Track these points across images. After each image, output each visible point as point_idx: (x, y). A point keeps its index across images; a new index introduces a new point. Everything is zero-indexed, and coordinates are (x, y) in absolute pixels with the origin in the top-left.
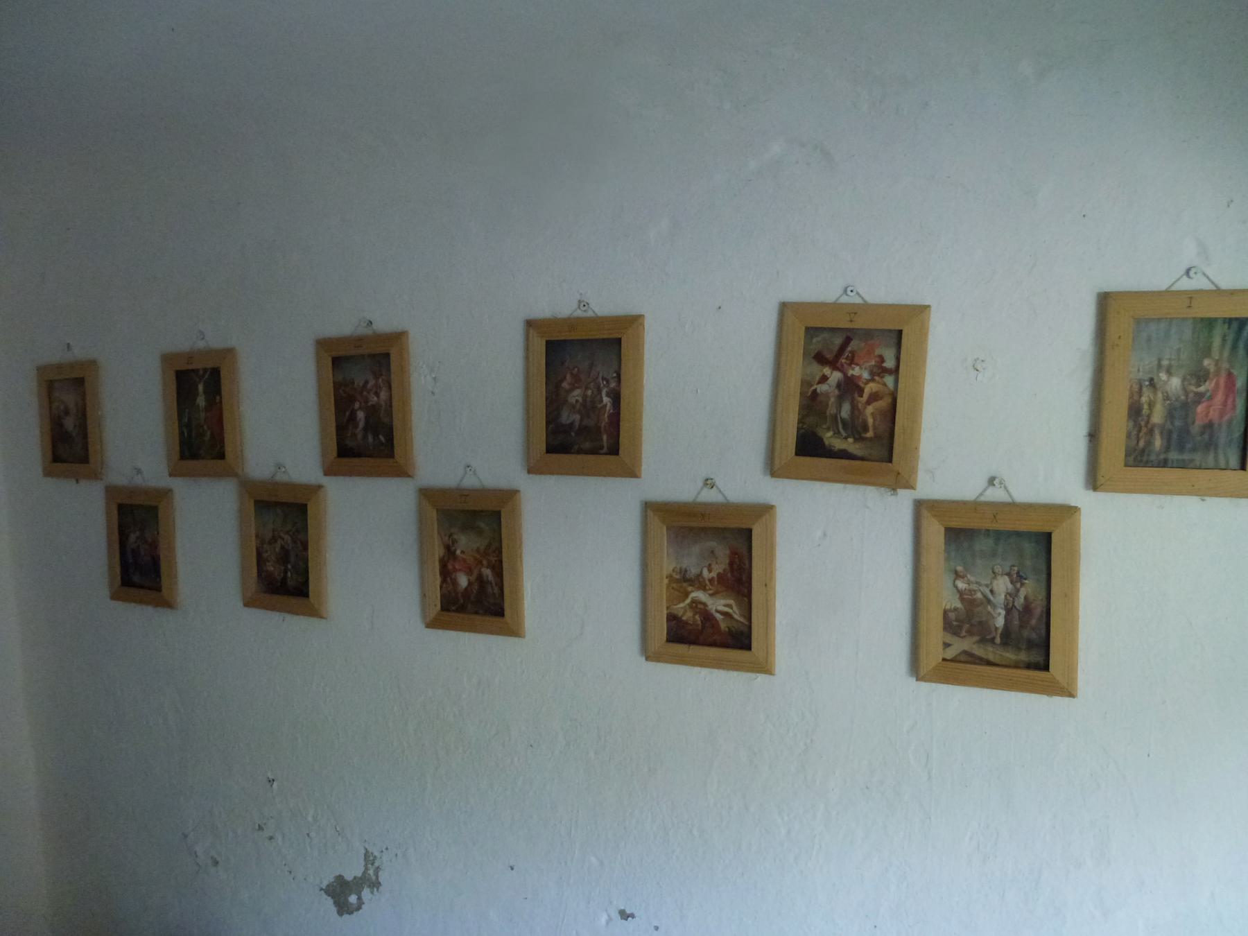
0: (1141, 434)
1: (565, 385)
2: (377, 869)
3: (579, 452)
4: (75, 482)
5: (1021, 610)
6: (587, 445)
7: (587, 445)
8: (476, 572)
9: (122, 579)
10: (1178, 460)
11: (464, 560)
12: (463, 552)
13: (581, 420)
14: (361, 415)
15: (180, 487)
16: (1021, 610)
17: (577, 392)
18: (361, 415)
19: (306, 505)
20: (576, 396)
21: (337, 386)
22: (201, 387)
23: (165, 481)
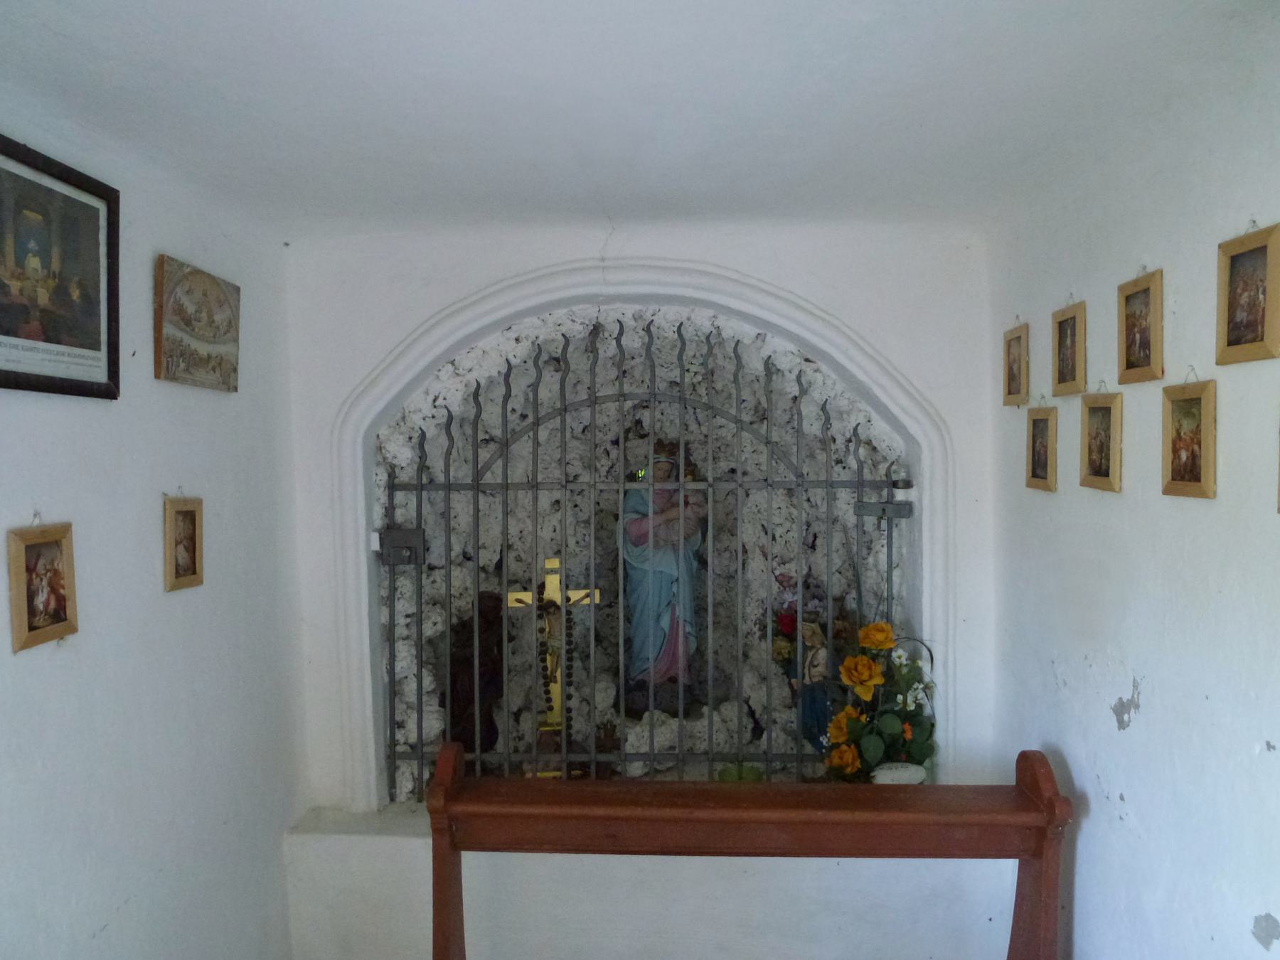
0: (731, 367)
1: (1239, 291)
2: (1139, 693)
3: (1245, 342)
4: (1017, 407)
5: (656, 752)
6: (1250, 336)
7: (1250, 336)
8: (1191, 449)
9: (1033, 474)
10: (533, 466)
11: (1185, 440)
12: (1185, 434)
13: (1248, 316)
14: (1138, 336)
15: (1124, 389)
16: (656, 752)
17: (1246, 294)
18: (1138, 336)
19: (1110, 408)
20: (1244, 299)
21: (1128, 317)
22: (1069, 332)
23: (1057, 402)
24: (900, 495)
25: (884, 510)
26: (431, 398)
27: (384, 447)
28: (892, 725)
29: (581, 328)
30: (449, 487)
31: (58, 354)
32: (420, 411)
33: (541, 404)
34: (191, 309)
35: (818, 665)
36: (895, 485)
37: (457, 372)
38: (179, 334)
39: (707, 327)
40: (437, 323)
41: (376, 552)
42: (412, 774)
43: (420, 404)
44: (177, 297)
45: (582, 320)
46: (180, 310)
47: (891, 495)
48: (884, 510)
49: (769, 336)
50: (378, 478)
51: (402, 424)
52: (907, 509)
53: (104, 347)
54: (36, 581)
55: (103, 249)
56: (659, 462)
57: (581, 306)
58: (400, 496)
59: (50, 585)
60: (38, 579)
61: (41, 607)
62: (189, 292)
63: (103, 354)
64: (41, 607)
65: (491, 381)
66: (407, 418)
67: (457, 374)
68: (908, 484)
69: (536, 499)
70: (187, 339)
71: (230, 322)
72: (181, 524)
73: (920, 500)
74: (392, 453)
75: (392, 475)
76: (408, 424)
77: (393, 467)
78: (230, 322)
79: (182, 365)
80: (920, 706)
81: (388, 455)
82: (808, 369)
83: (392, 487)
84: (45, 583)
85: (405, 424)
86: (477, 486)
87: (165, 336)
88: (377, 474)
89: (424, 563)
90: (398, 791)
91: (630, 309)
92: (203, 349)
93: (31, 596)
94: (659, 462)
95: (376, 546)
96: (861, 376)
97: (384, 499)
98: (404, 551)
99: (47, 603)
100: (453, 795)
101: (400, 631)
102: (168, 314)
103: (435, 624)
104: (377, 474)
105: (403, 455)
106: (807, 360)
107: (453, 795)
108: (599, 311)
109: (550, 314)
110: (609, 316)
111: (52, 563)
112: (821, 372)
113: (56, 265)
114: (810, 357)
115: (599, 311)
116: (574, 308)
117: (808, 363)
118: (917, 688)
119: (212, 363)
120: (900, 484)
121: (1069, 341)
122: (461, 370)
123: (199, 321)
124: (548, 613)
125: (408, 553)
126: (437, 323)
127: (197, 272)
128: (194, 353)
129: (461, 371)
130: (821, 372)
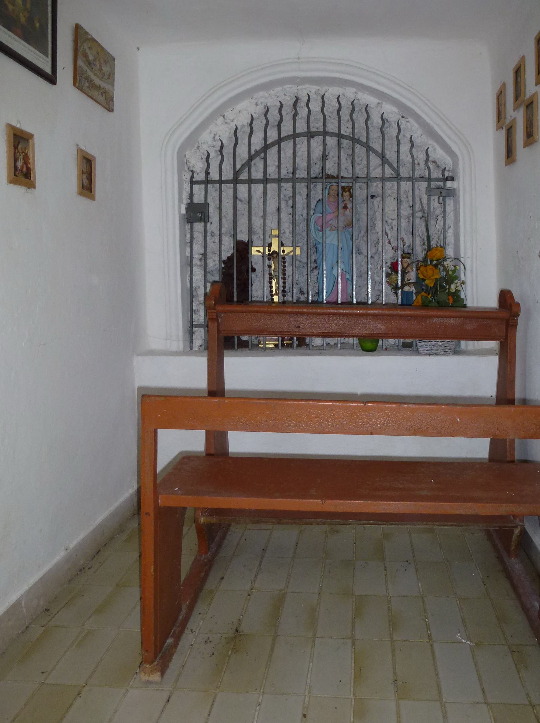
24: (449, 184)
25: (441, 192)
26: (212, 135)
27: (189, 161)
28: (442, 297)
29: (289, 99)
30: (221, 182)
31: (29, 49)
32: (207, 142)
33: (283, 233)
34: (91, 58)
35: (410, 280)
36: (447, 179)
37: (226, 121)
38: (85, 68)
39: (352, 97)
40: (215, 91)
41: (184, 215)
42: (201, 336)
43: (206, 137)
44: (85, 48)
45: (289, 94)
46: (85, 55)
47: (445, 185)
48: (441, 192)
49: (384, 103)
50: (185, 177)
51: (198, 150)
52: (452, 193)
53: (50, 56)
54: (18, 154)
55: (50, 9)
56: (332, 185)
57: (289, 86)
58: (196, 187)
59: (23, 158)
60: (19, 154)
61: (20, 168)
62: (90, 48)
63: (49, 59)
64: (20, 168)
65: (243, 126)
66: (200, 147)
67: (226, 123)
68: (452, 179)
69: (265, 172)
70: (89, 73)
71: (110, 74)
72: (85, 164)
73: (459, 187)
74: (192, 164)
75: (192, 177)
76: (201, 150)
77: (193, 172)
78: (110, 74)
79: (87, 84)
80: (457, 291)
81: (190, 165)
82: (403, 121)
83: (193, 182)
84: (21, 157)
85: (199, 150)
86: (235, 181)
87: (79, 65)
88: (184, 175)
89: (209, 222)
90: (194, 345)
91: (312, 89)
92: (97, 81)
93: (15, 160)
94: (332, 185)
95: (184, 211)
96: (428, 120)
97: (188, 189)
98: (198, 214)
99: (22, 168)
100: (218, 302)
101: (196, 261)
102: (80, 54)
103: (214, 261)
104: (184, 175)
105: (199, 166)
106: (403, 117)
107: (218, 302)
108: (298, 89)
109: (273, 91)
110: (303, 91)
111: (25, 148)
112: (409, 122)
113: (28, 6)
114: (404, 115)
115: (298, 89)
116: (286, 87)
117: (403, 119)
118: (457, 283)
119: (101, 91)
120: (449, 179)
121: (519, 79)
122: (228, 120)
123: (95, 66)
124: (274, 258)
125: (200, 215)
126: (215, 91)
127: (93, 40)
128: (92, 81)
129: (228, 121)
130: (409, 122)
